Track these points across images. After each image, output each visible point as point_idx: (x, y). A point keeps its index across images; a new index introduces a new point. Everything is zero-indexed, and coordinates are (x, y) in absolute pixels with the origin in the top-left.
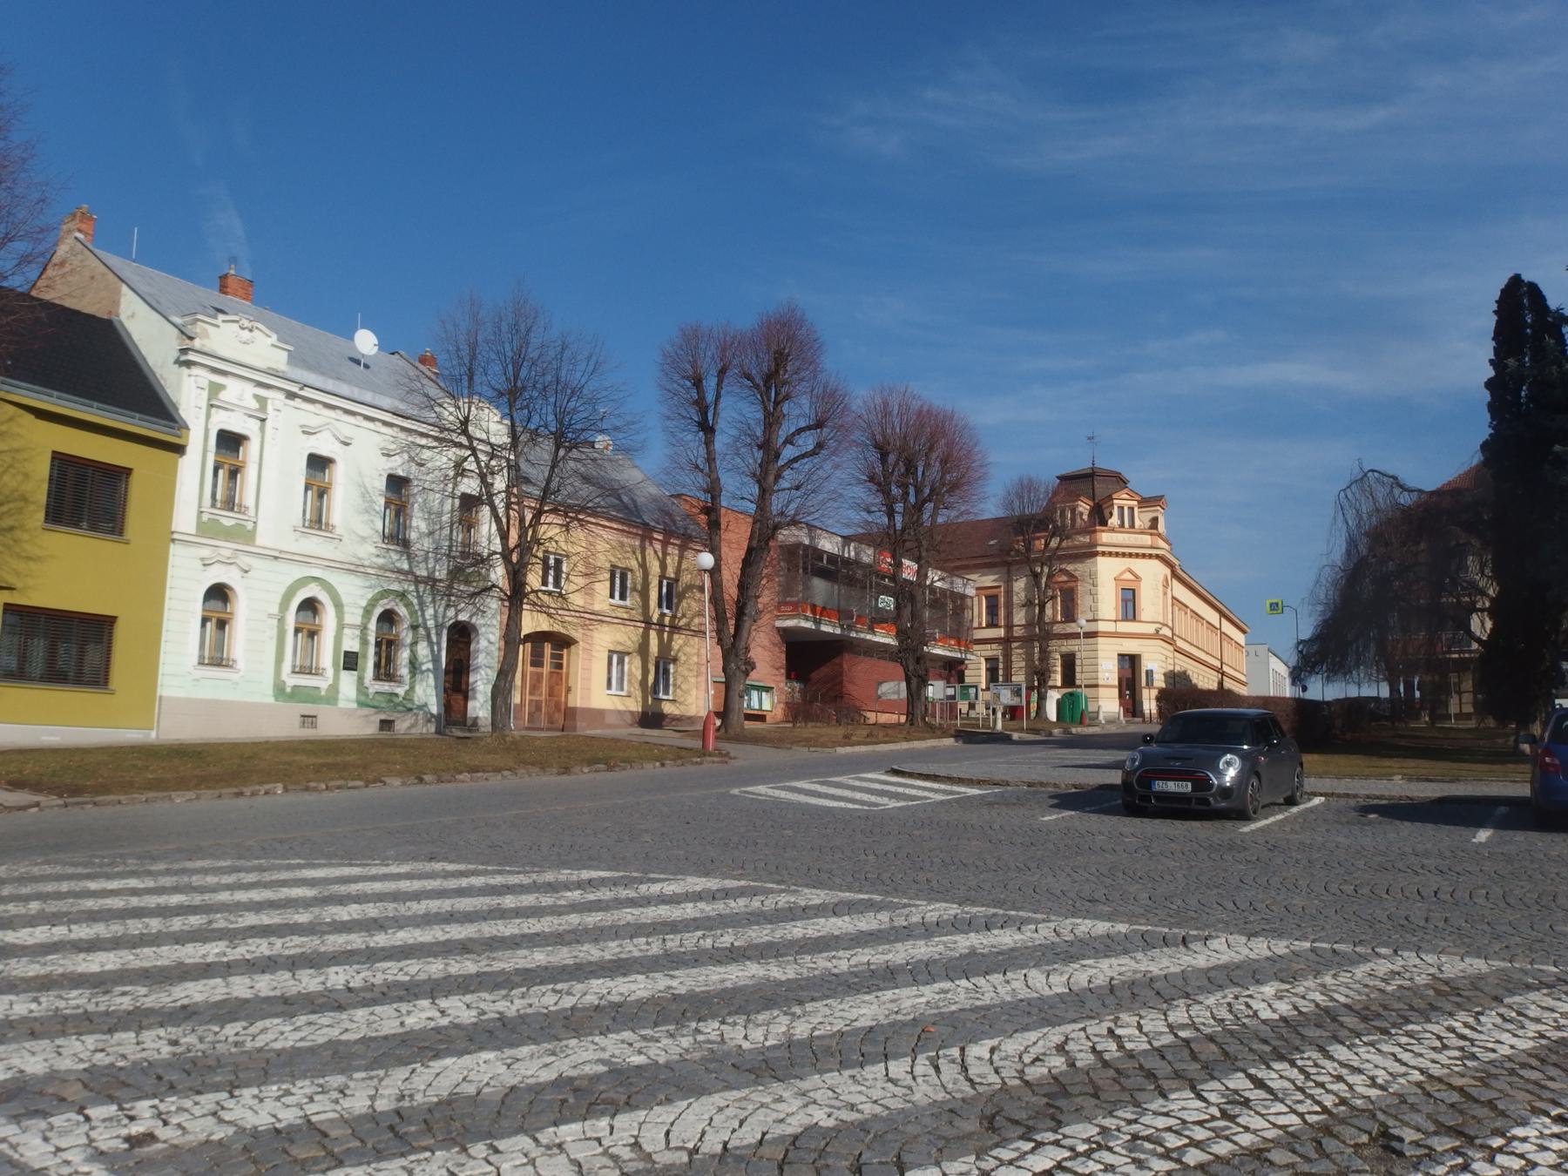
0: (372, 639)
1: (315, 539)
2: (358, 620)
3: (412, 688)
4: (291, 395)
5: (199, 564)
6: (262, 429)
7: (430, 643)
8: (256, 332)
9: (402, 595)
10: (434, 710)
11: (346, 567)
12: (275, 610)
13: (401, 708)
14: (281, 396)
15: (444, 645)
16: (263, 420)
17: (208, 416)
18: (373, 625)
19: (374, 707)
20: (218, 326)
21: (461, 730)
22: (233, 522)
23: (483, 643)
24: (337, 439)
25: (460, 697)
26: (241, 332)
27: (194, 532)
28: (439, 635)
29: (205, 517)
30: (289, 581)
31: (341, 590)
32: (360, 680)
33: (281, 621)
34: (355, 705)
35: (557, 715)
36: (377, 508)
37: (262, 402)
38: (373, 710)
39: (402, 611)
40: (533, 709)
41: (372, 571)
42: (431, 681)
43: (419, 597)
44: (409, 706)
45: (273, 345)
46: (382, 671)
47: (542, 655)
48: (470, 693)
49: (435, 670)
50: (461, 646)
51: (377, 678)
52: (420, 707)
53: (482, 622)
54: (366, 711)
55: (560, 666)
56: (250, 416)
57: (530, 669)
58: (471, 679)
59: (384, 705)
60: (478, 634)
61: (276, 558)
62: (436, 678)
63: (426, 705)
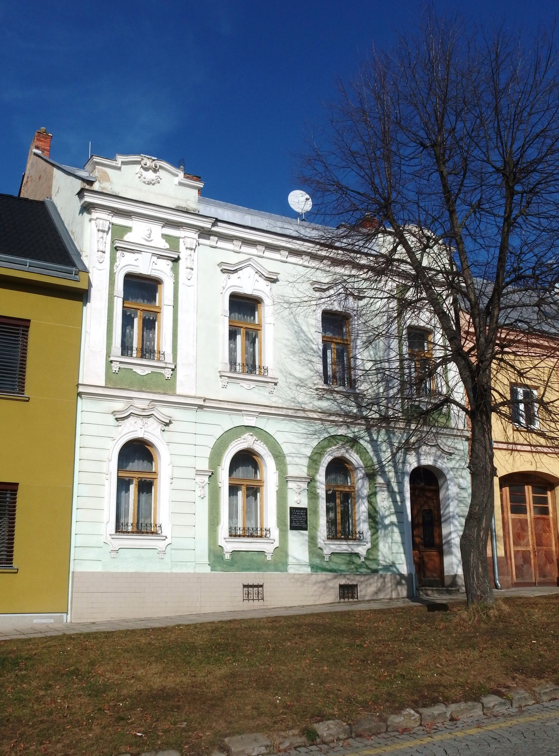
0: (322, 492)
1: (245, 384)
2: (303, 472)
3: (375, 546)
4: (204, 233)
5: (111, 419)
6: (175, 271)
7: (392, 493)
8: (161, 173)
9: (354, 442)
10: (404, 569)
11: (284, 412)
12: (204, 465)
13: (363, 570)
14: (194, 235)
15: (408, 495)
16: (176, 260)
17: (113, 260)
18: (321, 477)
19: (331, 571)
20: (119, 169)
21: (440, 592)
22: (148, 371)
23: (453, 490)
24: (261, 275)
25: (434, 553)
26: (145, 173)
27: (103, 384)
28: (400, 483)
29: (115, 367)
30: (219, 432)
31: (280, 438)
32: (313, 540)
33: (213, 476)
34: (309, 570)
35: (548, 567)
36: (315, 347)
37: (174, 242)
38: (330, 575)
39: (354, 458)
40: (521, 561)
41: (315, 416)
42: (397, 536)
43: (373, 442)
44: (374, 566)
45: (181, 184)
46: (339, 528)
47: (523, 500)
48: (445, 547)
49: (400, 523)
50: (429, 494)
51: (333, 536)
52: (387, 568)
53: (451, 465)
54: (322, 576)
55: (545, 511)
56: (160, 257)
57: (510, 516)
58: (445, 531)
59: (343, 567)
60: (446, 480)
61: (201, 407)
62: (402, 533)
63: (393, 565)
